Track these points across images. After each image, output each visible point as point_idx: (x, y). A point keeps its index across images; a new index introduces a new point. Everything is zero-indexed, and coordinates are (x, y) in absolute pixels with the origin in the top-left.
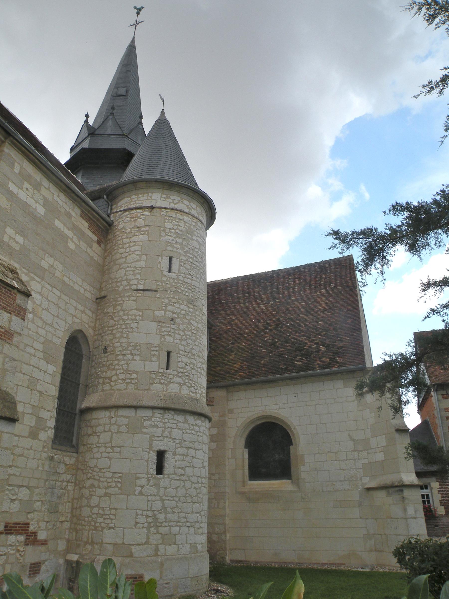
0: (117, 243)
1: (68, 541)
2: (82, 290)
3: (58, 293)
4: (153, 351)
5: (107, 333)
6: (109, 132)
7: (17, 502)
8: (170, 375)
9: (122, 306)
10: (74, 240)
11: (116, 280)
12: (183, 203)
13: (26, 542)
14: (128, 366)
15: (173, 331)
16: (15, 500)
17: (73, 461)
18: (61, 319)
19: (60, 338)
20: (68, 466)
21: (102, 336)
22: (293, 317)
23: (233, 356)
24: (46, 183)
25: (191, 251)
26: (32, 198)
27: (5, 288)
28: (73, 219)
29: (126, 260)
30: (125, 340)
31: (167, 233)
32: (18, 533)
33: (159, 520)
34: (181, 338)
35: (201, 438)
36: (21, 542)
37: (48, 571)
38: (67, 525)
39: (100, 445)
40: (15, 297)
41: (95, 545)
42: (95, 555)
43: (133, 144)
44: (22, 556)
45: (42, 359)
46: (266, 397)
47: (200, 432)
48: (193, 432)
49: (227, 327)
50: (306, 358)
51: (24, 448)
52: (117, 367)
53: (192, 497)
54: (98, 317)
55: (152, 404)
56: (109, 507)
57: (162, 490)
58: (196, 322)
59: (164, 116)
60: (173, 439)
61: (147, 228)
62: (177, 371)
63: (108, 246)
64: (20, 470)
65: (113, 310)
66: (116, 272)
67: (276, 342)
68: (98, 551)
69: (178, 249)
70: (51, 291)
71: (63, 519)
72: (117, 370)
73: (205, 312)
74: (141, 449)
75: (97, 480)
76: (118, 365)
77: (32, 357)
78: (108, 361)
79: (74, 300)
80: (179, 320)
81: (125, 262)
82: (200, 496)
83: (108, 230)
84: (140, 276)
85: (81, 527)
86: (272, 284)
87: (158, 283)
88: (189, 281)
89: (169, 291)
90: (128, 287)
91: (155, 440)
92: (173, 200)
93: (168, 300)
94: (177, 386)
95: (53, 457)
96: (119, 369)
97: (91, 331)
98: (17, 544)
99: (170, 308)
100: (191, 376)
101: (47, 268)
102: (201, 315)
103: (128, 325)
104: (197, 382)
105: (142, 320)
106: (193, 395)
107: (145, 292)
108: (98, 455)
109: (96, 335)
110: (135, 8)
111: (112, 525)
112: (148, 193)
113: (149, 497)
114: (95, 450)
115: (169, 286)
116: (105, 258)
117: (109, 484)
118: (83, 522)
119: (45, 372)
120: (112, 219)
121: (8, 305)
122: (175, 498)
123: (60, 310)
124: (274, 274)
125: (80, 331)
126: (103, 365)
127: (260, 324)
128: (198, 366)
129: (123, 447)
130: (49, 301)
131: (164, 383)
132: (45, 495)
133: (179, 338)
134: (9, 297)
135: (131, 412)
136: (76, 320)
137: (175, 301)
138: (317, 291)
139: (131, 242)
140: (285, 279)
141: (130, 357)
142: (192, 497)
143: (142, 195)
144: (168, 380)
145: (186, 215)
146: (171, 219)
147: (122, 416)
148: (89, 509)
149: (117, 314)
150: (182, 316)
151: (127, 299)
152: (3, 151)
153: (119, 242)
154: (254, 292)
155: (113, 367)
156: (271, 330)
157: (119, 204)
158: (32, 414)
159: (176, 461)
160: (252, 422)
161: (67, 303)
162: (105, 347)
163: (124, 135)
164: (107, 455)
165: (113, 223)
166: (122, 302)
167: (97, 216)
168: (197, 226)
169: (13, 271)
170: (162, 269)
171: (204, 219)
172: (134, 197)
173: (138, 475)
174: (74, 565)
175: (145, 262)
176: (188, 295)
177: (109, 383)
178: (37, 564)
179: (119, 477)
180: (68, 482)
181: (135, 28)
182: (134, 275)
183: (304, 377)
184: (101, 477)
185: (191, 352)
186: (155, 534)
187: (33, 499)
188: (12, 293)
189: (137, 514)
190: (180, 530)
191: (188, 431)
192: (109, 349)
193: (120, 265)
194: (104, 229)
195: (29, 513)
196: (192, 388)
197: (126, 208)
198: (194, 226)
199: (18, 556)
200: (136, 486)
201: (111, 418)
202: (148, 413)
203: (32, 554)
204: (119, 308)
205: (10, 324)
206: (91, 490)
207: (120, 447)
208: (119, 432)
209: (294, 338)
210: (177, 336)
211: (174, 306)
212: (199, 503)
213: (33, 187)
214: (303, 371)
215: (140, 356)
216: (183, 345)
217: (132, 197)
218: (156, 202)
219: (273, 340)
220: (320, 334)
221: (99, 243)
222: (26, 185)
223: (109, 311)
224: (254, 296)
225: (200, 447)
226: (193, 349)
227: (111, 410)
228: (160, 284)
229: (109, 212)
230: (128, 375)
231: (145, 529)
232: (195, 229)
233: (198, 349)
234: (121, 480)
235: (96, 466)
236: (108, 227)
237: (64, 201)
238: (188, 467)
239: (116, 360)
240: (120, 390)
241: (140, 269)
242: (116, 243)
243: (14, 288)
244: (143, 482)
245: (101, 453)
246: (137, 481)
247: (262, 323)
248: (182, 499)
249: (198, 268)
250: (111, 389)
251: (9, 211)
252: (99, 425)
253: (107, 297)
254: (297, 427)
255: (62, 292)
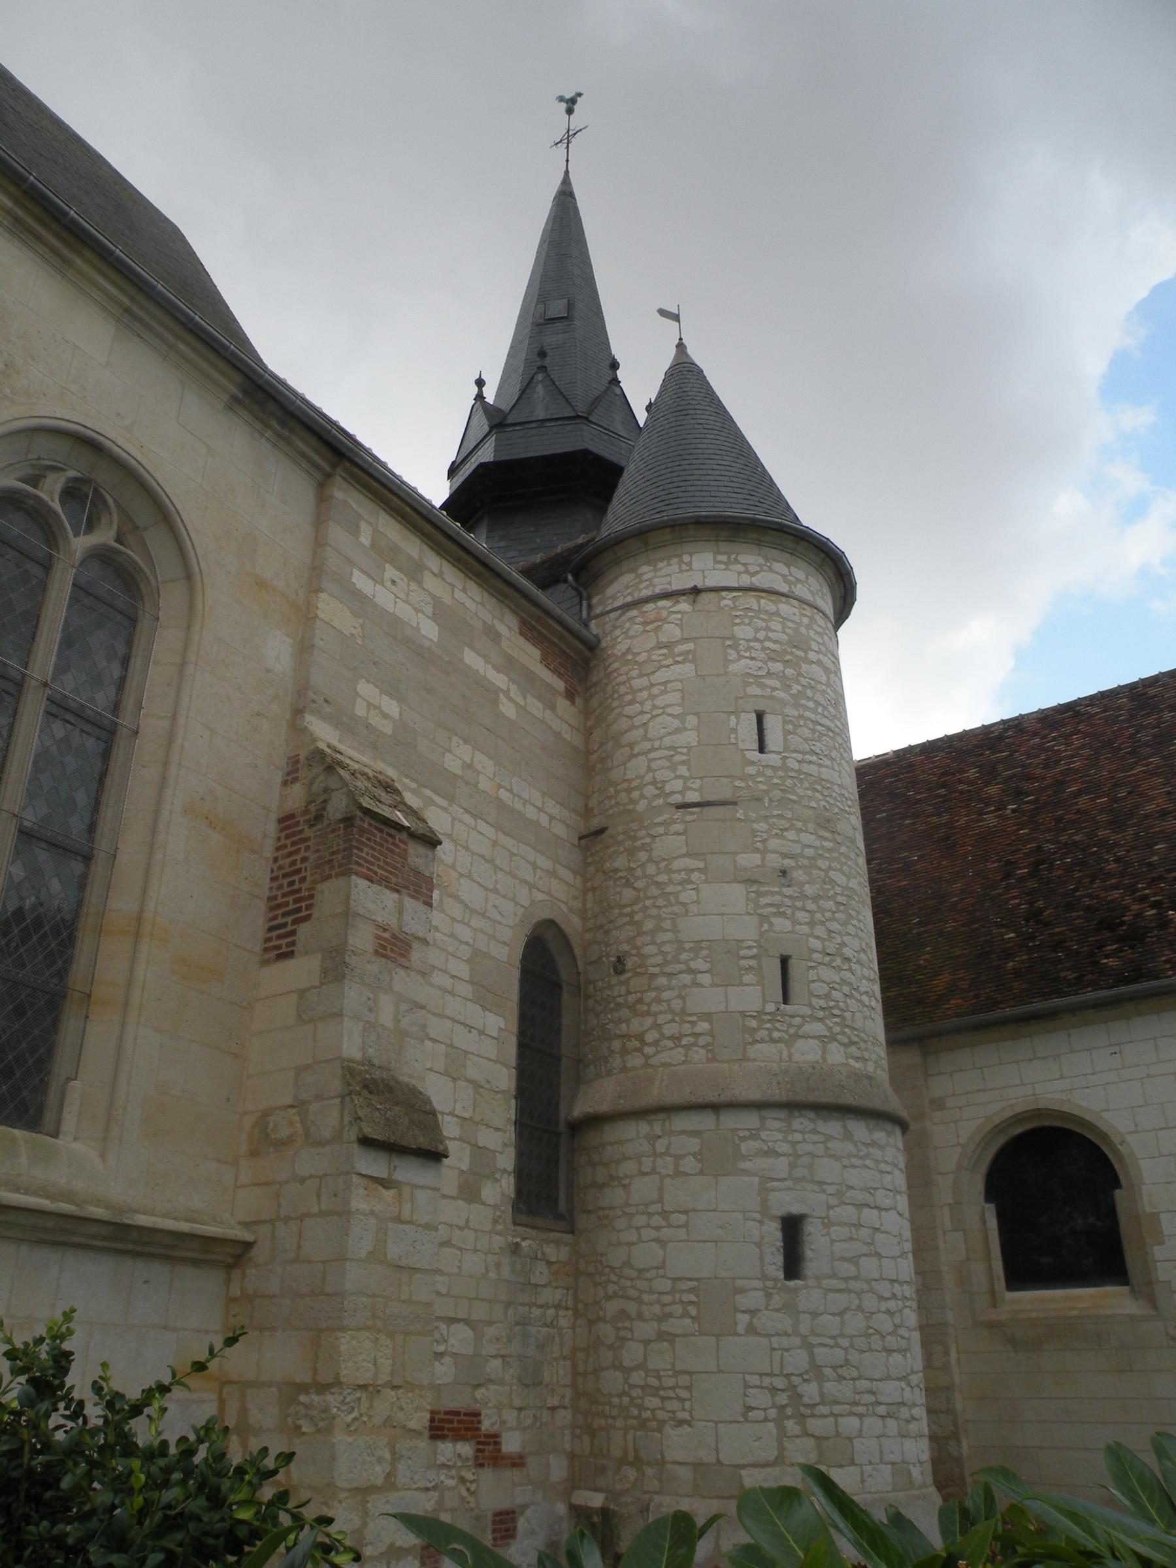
0: (617, 691)
1: (572, 1457)
2: (544, 820)
3: (490, 832)
4: (744, 958)
5: (620, 922)
6: (540, 414)
7: (447, 1359)
8: (791, 1017)
9: (650, 851)
10: (512, 694)
11: (625, 785)
12: (772, 571)
13: (476, 1458)
14: (684, 1003)
15: (788, 902)
16: (442, 1354)
17: (564, 1254)
18: (504, 897)
19: (505, 943)
20: (556, 1267)
21: (607, 932)
22: (1077, 838)
23: (928, 956)
24: (433, 561)
25: (809, 693)
26: (406, 602)
27: (381, 831)
28: (504, 643)
29: (646, 731)
30: (668, 936)
31: (742, 653)
32: (458, 1437)
33: (806, 1400)
34: (812, 918)
35: (889, 1178)
36: (467, 1459)
37: (533, 1532)
38: (564, 1417)
39: (633, 1210)
40: (405, 851)
41: (644, 1467)
42: (649, 1492)
43: (606, 437)
44: (472, 1494)
45: (471, 1000)
46: (1031, 1060)
47: (886, 1162)
48: (867, 1162)
49: (899, 881)
50: (1132, 947)
51: (451, 1226)
52: (655, 1008)
53: (883, 1337)
54: (589, 884)
55: (755, 1095)
56: (673, 1369)
57: (805, 1319)
58: (844, 874)
59: (687, 356)
60: (821, 1183)
61: (691, 646)
62: (810, 1005)
63: (595, 702)
64: (445, 1279)
65: (629, 861)
66: (624, 764)
67: (1040, 912)
68: (655, 1482)
69: (774, 689)
70: (475, 829)
71: (553, 1401)
72: (655, 1014)
73: (861, 845)
74: (740, 1216)
75: (634, 1299)
76: (658, 1000)
77: (449, 998)
78: (629, 993)
79: (528, 845)
80: (800, 872)
81: (645, 738)
82: (902, 1331)
83: (587, 661)
84: (689, 770)
85: (603, 1422)
86: (1007, 756)
87: (737, 784)
88: (813, 769)
89: (766, 800)
90: (661, 801)
91: (773, 1190)
92: (744, 565)
93: (767, 823)
94: (814, 1043)
95: (517, 1245)
96: (661, 1012)
97: (575, 920)
98: (459, 1464)
99: (774, 843)
100: (848, 1015)
101: (459, 772)
102: (853, 856)
103: (672, 898)
104: (864, 1032)
105: (706, 881)
106: (857, 1065)
107: (706, 809)
108: (631, 1236)
109: (590, 930)
110: (561, 99)
111: (684, 1415)
112: (680, 556)
113: (775, 1339)
114: (621, 1223)
115: (765, 787)
116: (588, 733)
117: (667, 1309)
118: (607, 1408)
119: (482, 1033)
120: (595, 632)
121: (390, 872)
122: (841, 1341)
123: (500, 875)
124: (1009, 728)
125: (550, 923)
126: (619, 1006)
127: (990, 866)
128: (862, 990)
129: (694, 1210)
130: (473, 854)
131: (780, 1040)
132: (509, 1341)
133: (807, 920)
134: (392, 852)
135: (704, 1121)
136: (540, 896)
137: (783, 823)
138: (1136, 763)
139: (652, 685)
140: (1042, 738)
141: (686, 978)
142: (883, 1337)
143: (665, 563)
144: (792, 1031)
145: (784, 599)
146: (747, 616)
147: (683, 1132)
148: (619, 1374)
149: (639, 872)
150: (806, 862)
151: (661, 830)
152: (332, 497)
153: (622, 689)
154: (960, 782)
155: (645, 1008)
156: (1022, 879)
157: (610, 591)
158: (461, 1139)
159: (833, 1241)
160: (999, 1129)
161: (513, 855)
162: (619, 957)
163: (578, 417)
164: (653, 1234)
165: (599, 641)
166: (648, 840)
167: (560, 629)
168: (815, 627)
169: (388, 787)
170: (741, 746)
171: (828, 606)
172: (645, 569)
173: (738, 1282)
174: (596, 1519)
175: (695, 733)
176: (814, 805)
177: (640, 1050)
178: (507, 1513)
179: (692, 1290)
180: (558, 1307)
181: (567, 147)
182: (673, 767)
183: (1131, 998)
184: (645, 1292)
185: (839, 953)
186: (797, 1436)
187: (484, 1353)
188: (397, 841)
189: (747, 1386)
190: (861, 1424)
191: (855, 1161)
192: (629, 964)
193: (631, 745)
194: (578, 660)
195: (477, 1386)
196: (853, 1049)
197: (629, 599)
198: (808, 627)
199: (465, 1493)
200: (736, 1310)
201: (653, 1138)
202: (750, 1120)
203: (494, 1490)
204: (643, 856)
205: (400, 920)
206: (619, 1325)
207: (686, 1212)
208: (678, 1173)
209: (1090, 896)
210: (801, 915)
211: (783, 838)
212: (903, 1351)
213: (406, 574)
214: (1129, 981)
215: (712, 975)
216: (818, 937)
217: (640, 571)
218: (704, 577)
219: (1031, 904)
220: (1161, 878)
221: (570, 695)
222: (390, 572)
223: (617, 864)
224: (961, 792)
225: (887, 1202)
226: (844, 944)
227: (652, 1117)
228: (743, 784)
229: (585, 613)
230: (688, 1025)
231: (772, 1424)
232: (812, 633)
233: (856, 944)
234: (697, 1296)
235: (627, 1264)
236: (587, 653)
237: (478, 599)
238: (865, 1255)
239: (650, 989)
240: (670, 1065)
241: (685, 750)
242: (614, 692)
243: (400, 827)
244: (754, 1299)
245: (638, 1229)
246: (738, 1298)
247: (994, 862)
248: (860, 1342)
249: (831, 734)
250: (647, 1065)
251: (359, 641)
252: (626, 1158)
253: (608, 832)
254: (1129, 1138)
255: (498, 827)
